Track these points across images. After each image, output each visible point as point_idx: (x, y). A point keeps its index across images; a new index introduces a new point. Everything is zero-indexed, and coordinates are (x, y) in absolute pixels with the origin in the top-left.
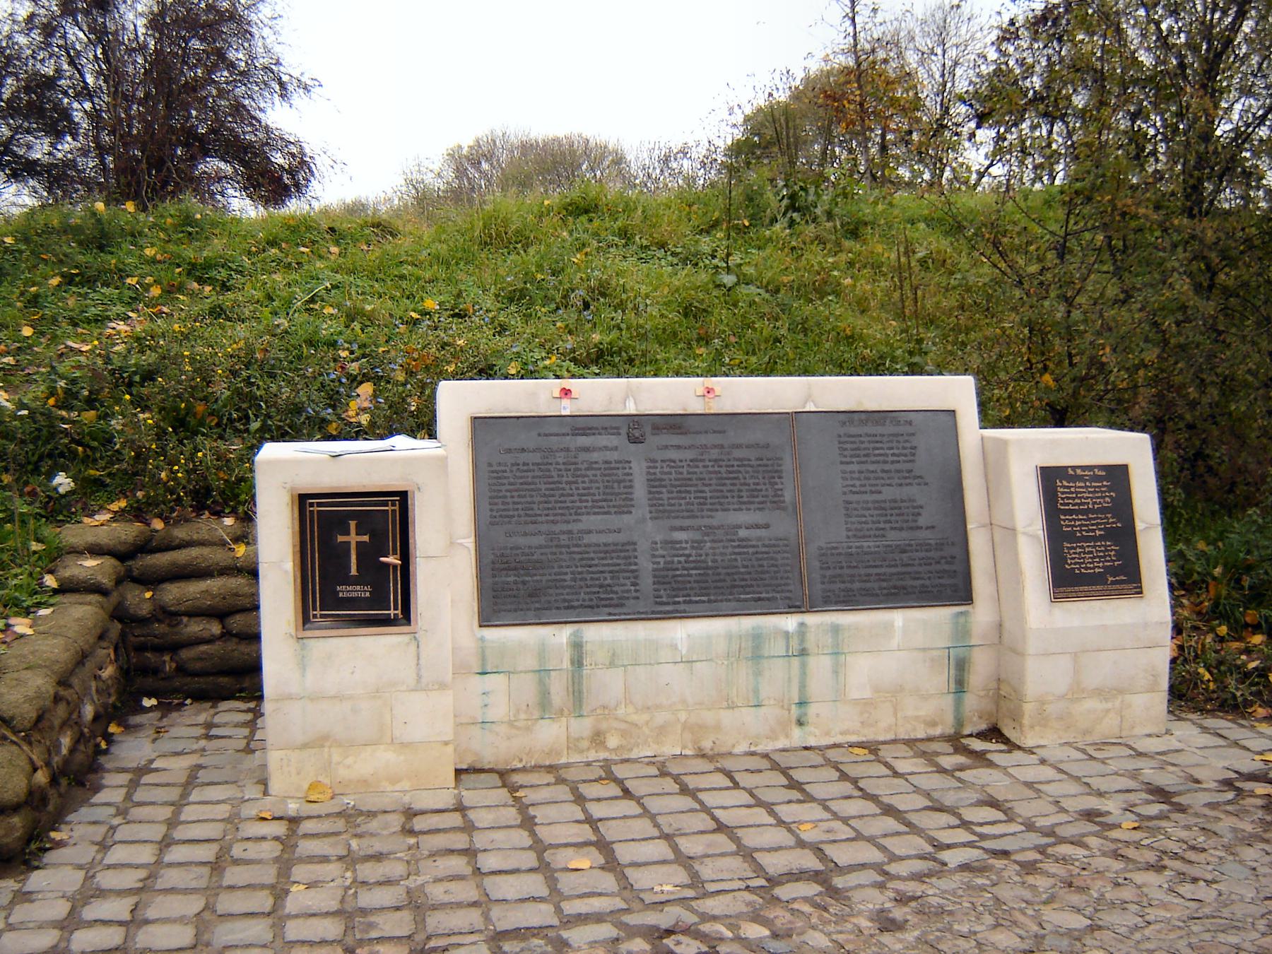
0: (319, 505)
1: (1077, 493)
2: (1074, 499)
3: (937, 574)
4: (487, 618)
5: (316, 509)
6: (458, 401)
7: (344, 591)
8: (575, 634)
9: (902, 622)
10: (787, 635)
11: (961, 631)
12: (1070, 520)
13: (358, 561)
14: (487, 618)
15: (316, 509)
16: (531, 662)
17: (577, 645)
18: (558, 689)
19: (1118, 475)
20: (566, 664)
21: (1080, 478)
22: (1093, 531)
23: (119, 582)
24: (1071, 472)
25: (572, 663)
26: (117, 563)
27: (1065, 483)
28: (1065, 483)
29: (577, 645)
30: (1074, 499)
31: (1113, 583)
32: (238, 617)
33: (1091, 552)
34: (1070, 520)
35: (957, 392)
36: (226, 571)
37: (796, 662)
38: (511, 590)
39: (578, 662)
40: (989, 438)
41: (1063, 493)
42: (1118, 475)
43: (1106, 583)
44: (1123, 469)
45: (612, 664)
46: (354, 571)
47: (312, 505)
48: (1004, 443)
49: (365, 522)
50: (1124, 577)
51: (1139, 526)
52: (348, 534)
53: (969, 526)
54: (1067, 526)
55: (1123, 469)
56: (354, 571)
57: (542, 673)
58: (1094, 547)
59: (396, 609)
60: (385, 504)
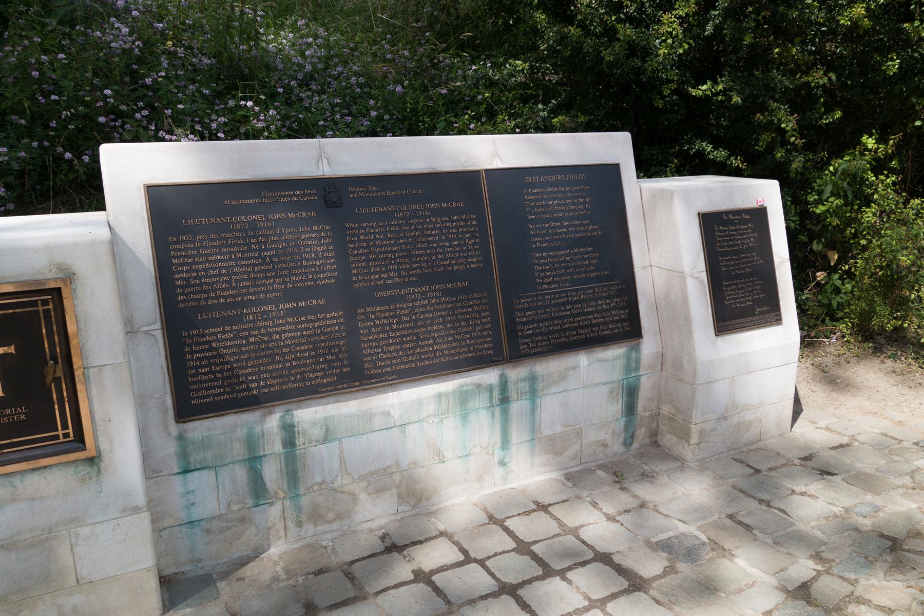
1: (730, 235)
2: (727, 241)
3: (605, 309)
6: (132, 167)
9: (584, 363)
11: (632, 366)
12: (726, 261)
17: (290, 433)
21: (732, 223)
22: (743, 269)
24: (725, 217)
27: (721, 228)
28: (721, 228)
30: (727, 241)
31: (760, 313)
33: (742, 288)
34: (726, 261)
38: (204, 377)
41: (720, 237)
43: (755, 315)
44: (617, 166)
50: (766, 311)
52: (57, 430)
54: (725, 266)
55: (617, 166)
58: (745, 283)
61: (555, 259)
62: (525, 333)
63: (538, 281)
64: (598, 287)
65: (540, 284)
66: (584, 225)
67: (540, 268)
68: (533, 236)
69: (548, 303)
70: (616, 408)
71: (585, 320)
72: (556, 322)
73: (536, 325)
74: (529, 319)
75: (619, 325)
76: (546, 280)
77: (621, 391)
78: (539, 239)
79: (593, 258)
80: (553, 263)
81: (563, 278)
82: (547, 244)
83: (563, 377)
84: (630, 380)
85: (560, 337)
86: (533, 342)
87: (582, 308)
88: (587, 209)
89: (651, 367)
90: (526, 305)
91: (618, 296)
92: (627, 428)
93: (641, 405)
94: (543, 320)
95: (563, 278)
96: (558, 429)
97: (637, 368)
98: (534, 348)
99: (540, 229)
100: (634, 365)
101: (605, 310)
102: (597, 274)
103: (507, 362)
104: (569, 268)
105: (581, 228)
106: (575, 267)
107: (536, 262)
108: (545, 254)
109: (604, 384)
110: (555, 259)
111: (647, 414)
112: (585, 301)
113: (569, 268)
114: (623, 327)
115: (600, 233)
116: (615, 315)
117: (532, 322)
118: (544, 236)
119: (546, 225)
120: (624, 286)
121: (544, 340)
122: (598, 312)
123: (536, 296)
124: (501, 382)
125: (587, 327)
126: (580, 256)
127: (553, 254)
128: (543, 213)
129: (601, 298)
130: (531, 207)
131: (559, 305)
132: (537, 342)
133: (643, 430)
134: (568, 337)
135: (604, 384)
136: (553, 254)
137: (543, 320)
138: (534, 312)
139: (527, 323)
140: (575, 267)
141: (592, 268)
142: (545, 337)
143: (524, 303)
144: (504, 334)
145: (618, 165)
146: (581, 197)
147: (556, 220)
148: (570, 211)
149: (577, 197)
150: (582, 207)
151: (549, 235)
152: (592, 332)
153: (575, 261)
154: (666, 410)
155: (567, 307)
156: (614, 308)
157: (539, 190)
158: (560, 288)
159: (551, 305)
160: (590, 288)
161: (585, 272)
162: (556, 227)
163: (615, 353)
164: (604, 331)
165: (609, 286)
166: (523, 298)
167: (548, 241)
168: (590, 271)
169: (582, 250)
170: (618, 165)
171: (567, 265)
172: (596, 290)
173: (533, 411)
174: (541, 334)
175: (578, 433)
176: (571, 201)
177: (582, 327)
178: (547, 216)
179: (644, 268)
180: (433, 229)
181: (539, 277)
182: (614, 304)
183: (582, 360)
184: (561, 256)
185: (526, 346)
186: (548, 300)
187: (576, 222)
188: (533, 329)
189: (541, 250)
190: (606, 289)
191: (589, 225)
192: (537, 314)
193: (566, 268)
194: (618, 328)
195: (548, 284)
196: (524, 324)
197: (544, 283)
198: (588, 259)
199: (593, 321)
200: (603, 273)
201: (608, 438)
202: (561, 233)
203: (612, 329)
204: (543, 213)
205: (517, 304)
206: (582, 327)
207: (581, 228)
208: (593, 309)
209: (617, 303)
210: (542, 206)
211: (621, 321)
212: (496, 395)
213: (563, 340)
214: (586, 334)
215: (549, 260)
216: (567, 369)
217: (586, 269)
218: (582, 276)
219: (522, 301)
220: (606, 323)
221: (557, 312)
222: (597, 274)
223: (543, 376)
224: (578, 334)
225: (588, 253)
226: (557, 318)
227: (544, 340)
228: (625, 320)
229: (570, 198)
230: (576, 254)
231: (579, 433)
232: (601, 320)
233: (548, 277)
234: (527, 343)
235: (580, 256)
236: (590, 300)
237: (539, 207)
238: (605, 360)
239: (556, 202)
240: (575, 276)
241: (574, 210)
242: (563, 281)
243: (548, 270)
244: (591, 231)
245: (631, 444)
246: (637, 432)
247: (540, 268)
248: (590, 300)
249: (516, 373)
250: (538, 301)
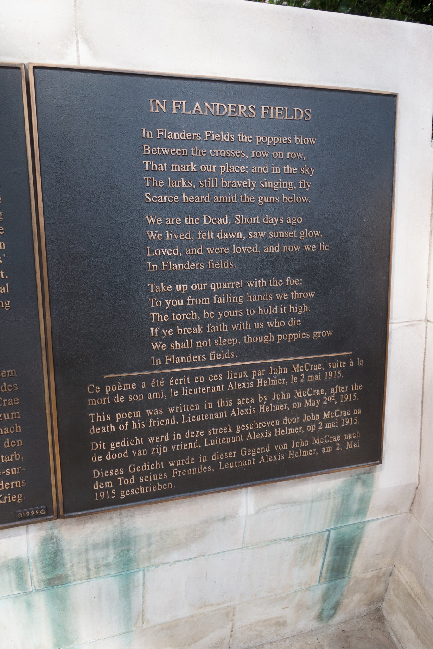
11: (350, 509)
61: (206, 300)
62: (109, 457)
63: (155, 346)
64: (301, 362)
65: (160, 354)
66: (286, 227)
67: (165, 318)
68: (156, 244)
69: (175, 394)
70: (310, 574)
71: (261, 430)
72: (189, 434)
73: (138, 441)
74: (124, 427)
75: (336, 439)
76: (176, 345)
77: (322, 548)
78: (169, 252)
79: (299, 302)
80: (199, 309)
81: (222, 341)
82: (189, 266)
83: (197, 534)
84: (344, 530)
85: (196, 465)
86: (127, 475)
87: (256, 405)
88: (300, 192)
89: (390, 508)
90: (119, 399)
91: (340, 382)
92: (325, 597)
93: (358, 566)
94: (158, 431)
95: (222, 341)
96: (184, 612)
97: (362, 511)
98: (130, 487)
99: (175, 229)
100: (355, 507)
101: (310, 410)
102: (303, 335)
103: (58, 517)
104: (236, 320)
105: (281, 234)
106: (253, 319)
107: (155, 303)
108: (182, 288)
109: (289, 540)
110: (206, 300)
111: (369, 575)
112: (268, 391)
113: (236, 320)
114: (343, 442)
115: (324, 248)
116: (330, 420)
117: (131, 434)
118: (183, 245)
119: (191, 221)
120: (360, 363)
121: (157, 472)
122: (292, 413)
123: (148, 379)
124: (43, 553)
125: (262, 443)
126: (268, 297)
127: (201, 287)
128: (189, 191)
129: (304, 387)
130: (157, 174)
131: (200, 399)
132: (137, 475)
133: (357, 597)
134: (215, 465)
135: (289, 540)
136: (201, 287)
137: (158, 431)
138: (137, 414)
139: (117, 436)
140: (253, 319)
141: (292, 323)
142: (158, 465)
143: (113, 394)
144: (55, 458)
145: (394, 96)
146: (292, 162)
147: (219, 210)
148: (259, 191)
149: (281, 162)
150: (290, 185)
151: (196, 244)
152: (273, 452)
153: (254, 305)
154: (404, 576)
155: (222, 403)
156: (331, 407)
157: (185, 135)
158: (209, 362)
159: (182, 400)
160: (283, 364)
161: (275, 331)
162: (216, 228)
163: (305, 502)
164: (301, 450)
165: (325, 362)
166: (113, 381)
167: (194, 259)
168: (288, 330)
169: (275, 282)
170: (394, 96)
171: (232, 314)
172: (295, 368)
173: (126, 592)
174: (150, 459)
175: (227, 614)
176: (264, 169)
177: (251, 445)
178: (199, 199)
179: (412, 324)
180: (185, 309)
181: (159, 338)
182: (332, 398)
183: (245, 503)
184: (221, 293)
185: (109, 484)
186: (178, 388)
187: (268, 220)
188: (131, 449)
189: (173, 277)
190: (318, 367)
191: (299, 227)
192: (145, 418)
193: (229, 321)
194: (334, 445)
195: (179, 353)
196: (108, 438)
197: (169, 351)
198: (287, 303)
199: (278, 432)
200: (318, 334)
201: (289, 614)
202: (228, 243)
203: (319, 448)
204: (189, 191)
205: (95, 396)
206: (251, 445)
207: (281, 234)
208: (283, 407)
209: (338, 396)
210: (188, 175)
211: (341, 431)
212: (35, 575)
213: (203, 469)
214: (258, 457)
215: (191, 300)
216: (207, 522)
217: (278, 324)
218: (266, 339)
219: (108, 389)
220: (307, 436)
221: (195, 413)
222: (303, 335)
223: (149, 537)
224: (239, 457)
225: (289, 289)
226: (194, 427)
227: (157, 472)
228: (350, 429)
229: (262, 161)
230: (261, 291)
231: (229, 614)
232: (298, 430)
233: (182, 338)
234: (114, 479)
235: (268, 297)
236: (278, 389)
237: (179, 174)
238: (293, 503)
239: (224, 168)
240: (249, 339)
241: (269, 191)
242: (218, 350)
243: (183, 324)
244: (302, 243)
245: (331, 617)
246: (346, 601)
247: (165, 318)
248: (278, 389)
249: (81, 535)
250: (150, 390)
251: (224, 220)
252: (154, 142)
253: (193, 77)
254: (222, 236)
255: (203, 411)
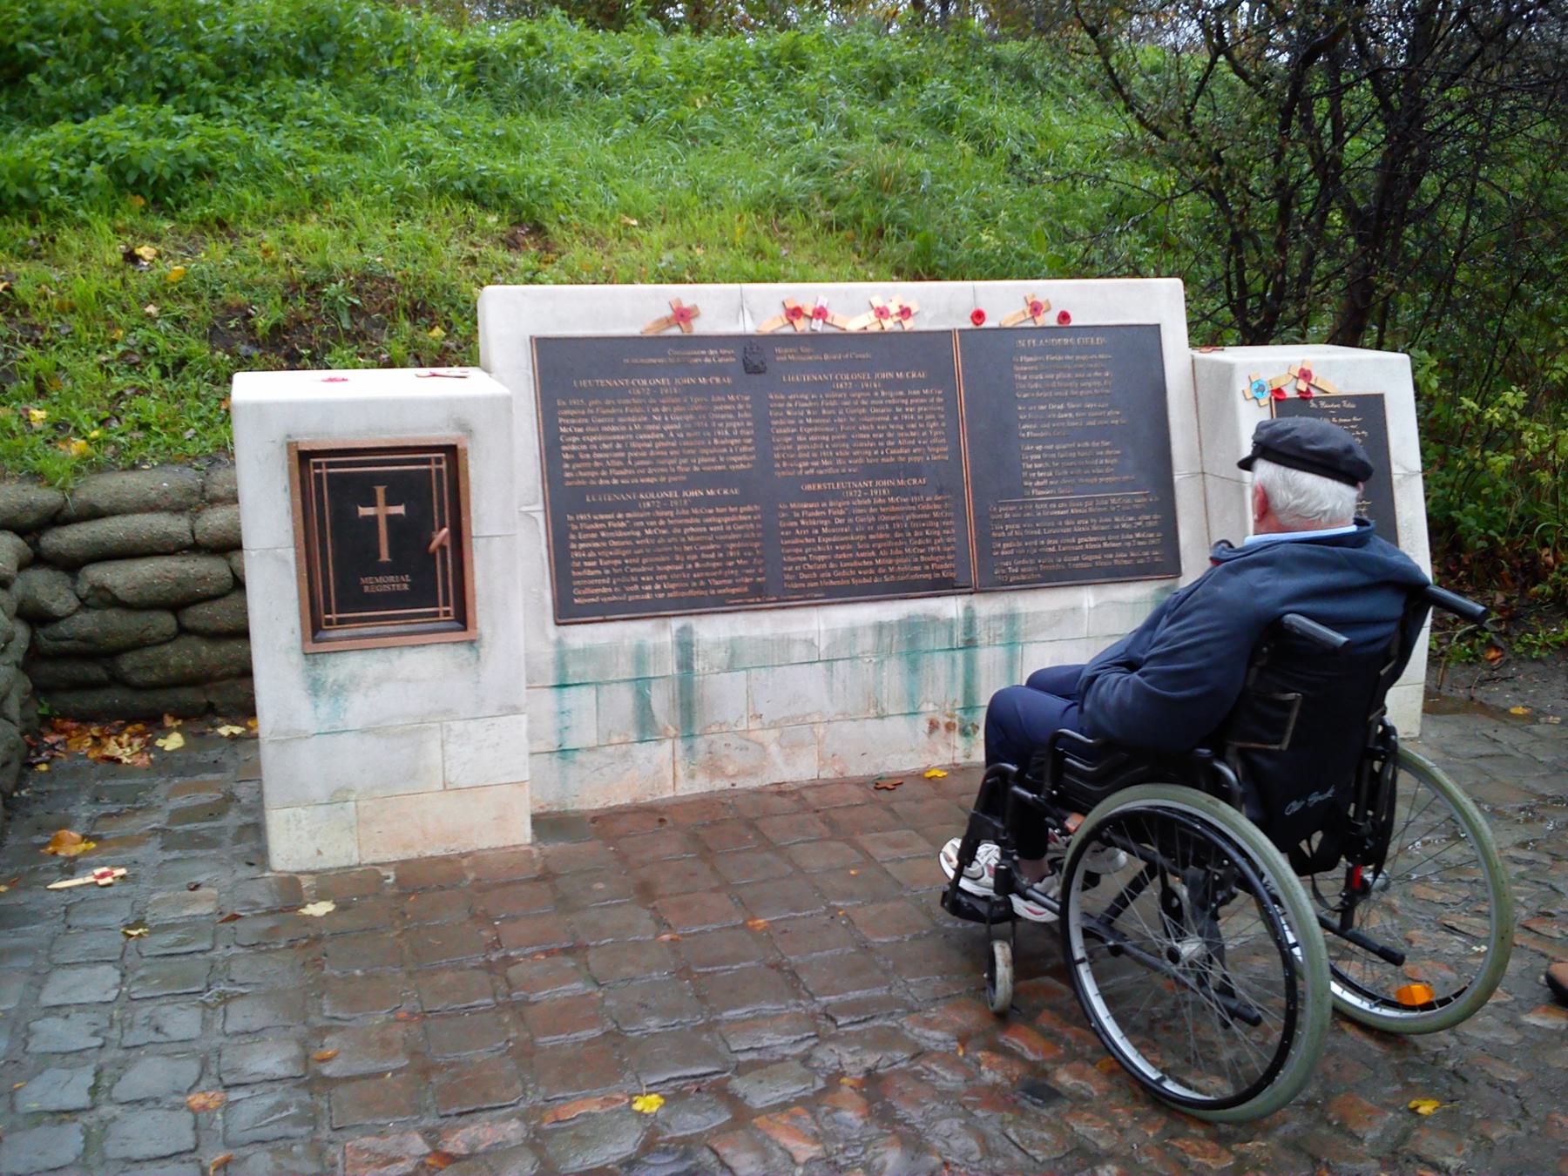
0: (330, 465)
4: (568, 611)
5: (324, 471)
6: (513, 314)
7: (375, 584)
8: (685, 630)
10: (950, 624)
13: (388, 543)
14: (568, 611)
15: (324, 471)
16: (625, 669)
18: (661, 701)
19: (1371, 408)
20: (671, 668)
23: (22, 567)
25: (680, 667)
26: (18, 541)
29: (686, 649)
32: (208, 617)
35: (1160, 302)
36: (195, 548)
37: (959, 655)
39: (686, 664)
40: (1203, 361)
42: (1371, 408)
45: (730, 668)
46: (385, 556)
47: (318, 466)
48: (1229, 369)
49: (399, 488)
51: (1396, 470)
53: (1176, 478)
56: (385, 556)
57: (641, 684)
59: (446, 604)
60: (427, 461)
106: (1083, 467)
108: (1039, 448)
123: (1023, 503)
127: (1050, 447)
136: (1050, 447)
137: (1032, 538)
142: (1032, 562)
156: (1139, 529)
162: (1057, 411)
193: (1068, 468)
225: (1105, 448)
226: (1053, 536)
233: (1041, 479)
242: (1063, 486)
251: (1061, 407)
252: (1020, 364)
253: (299, 501)
254: (1061, 416)
255: (1057, 527)
